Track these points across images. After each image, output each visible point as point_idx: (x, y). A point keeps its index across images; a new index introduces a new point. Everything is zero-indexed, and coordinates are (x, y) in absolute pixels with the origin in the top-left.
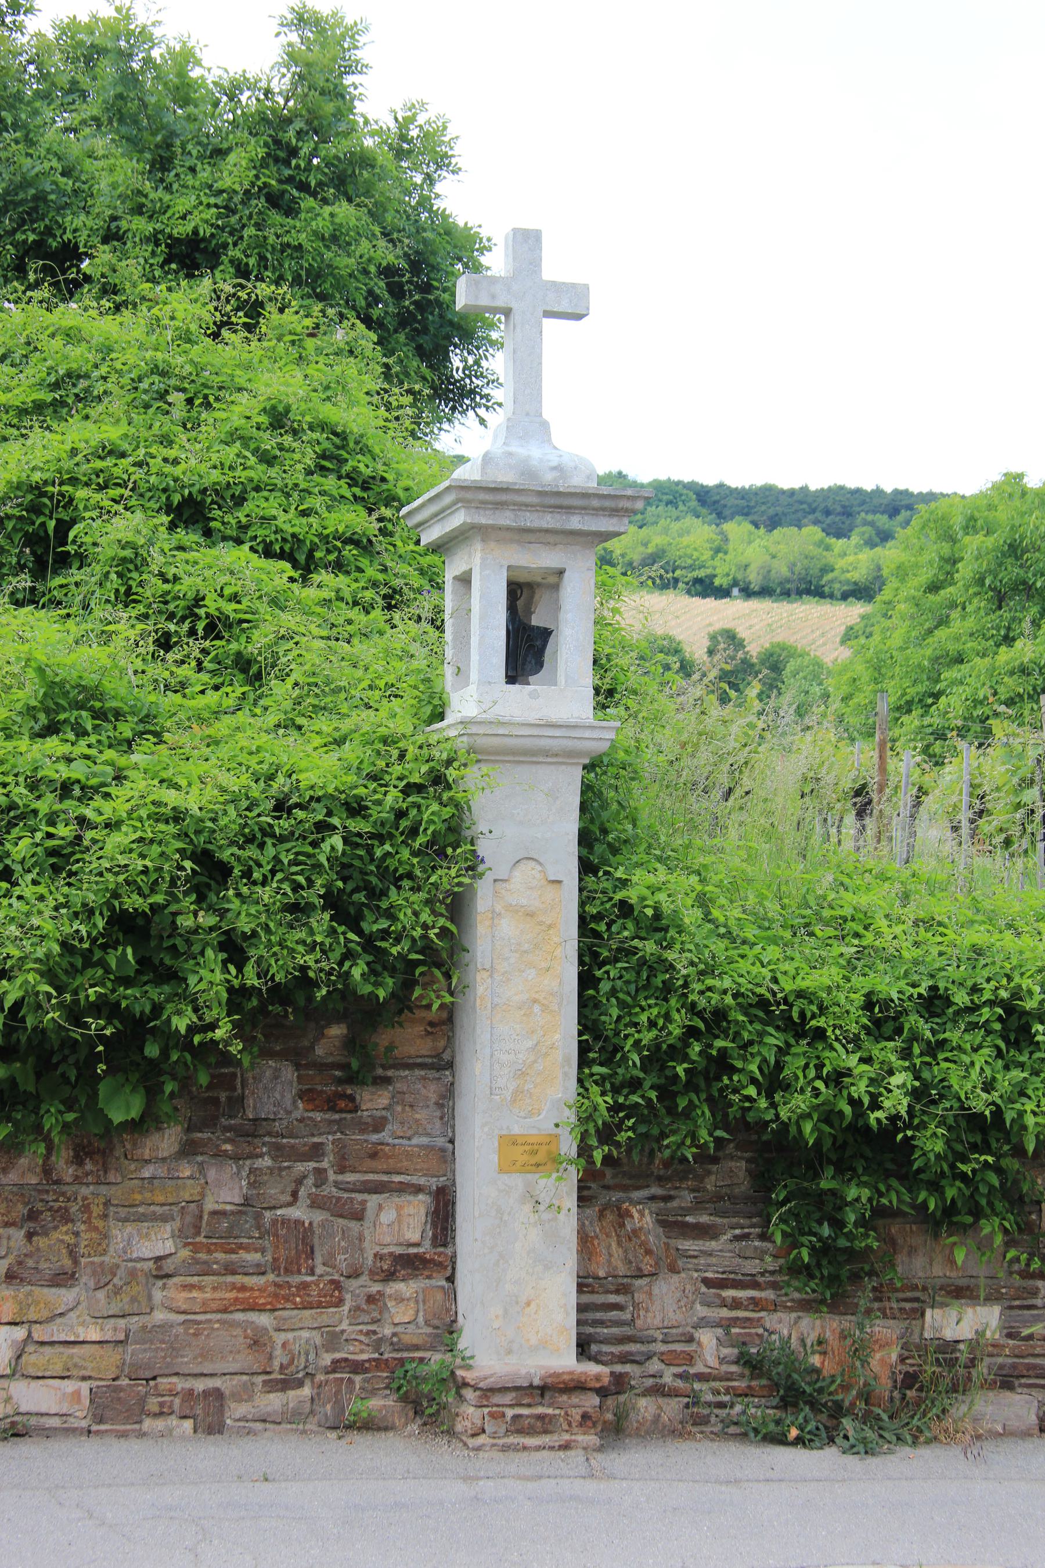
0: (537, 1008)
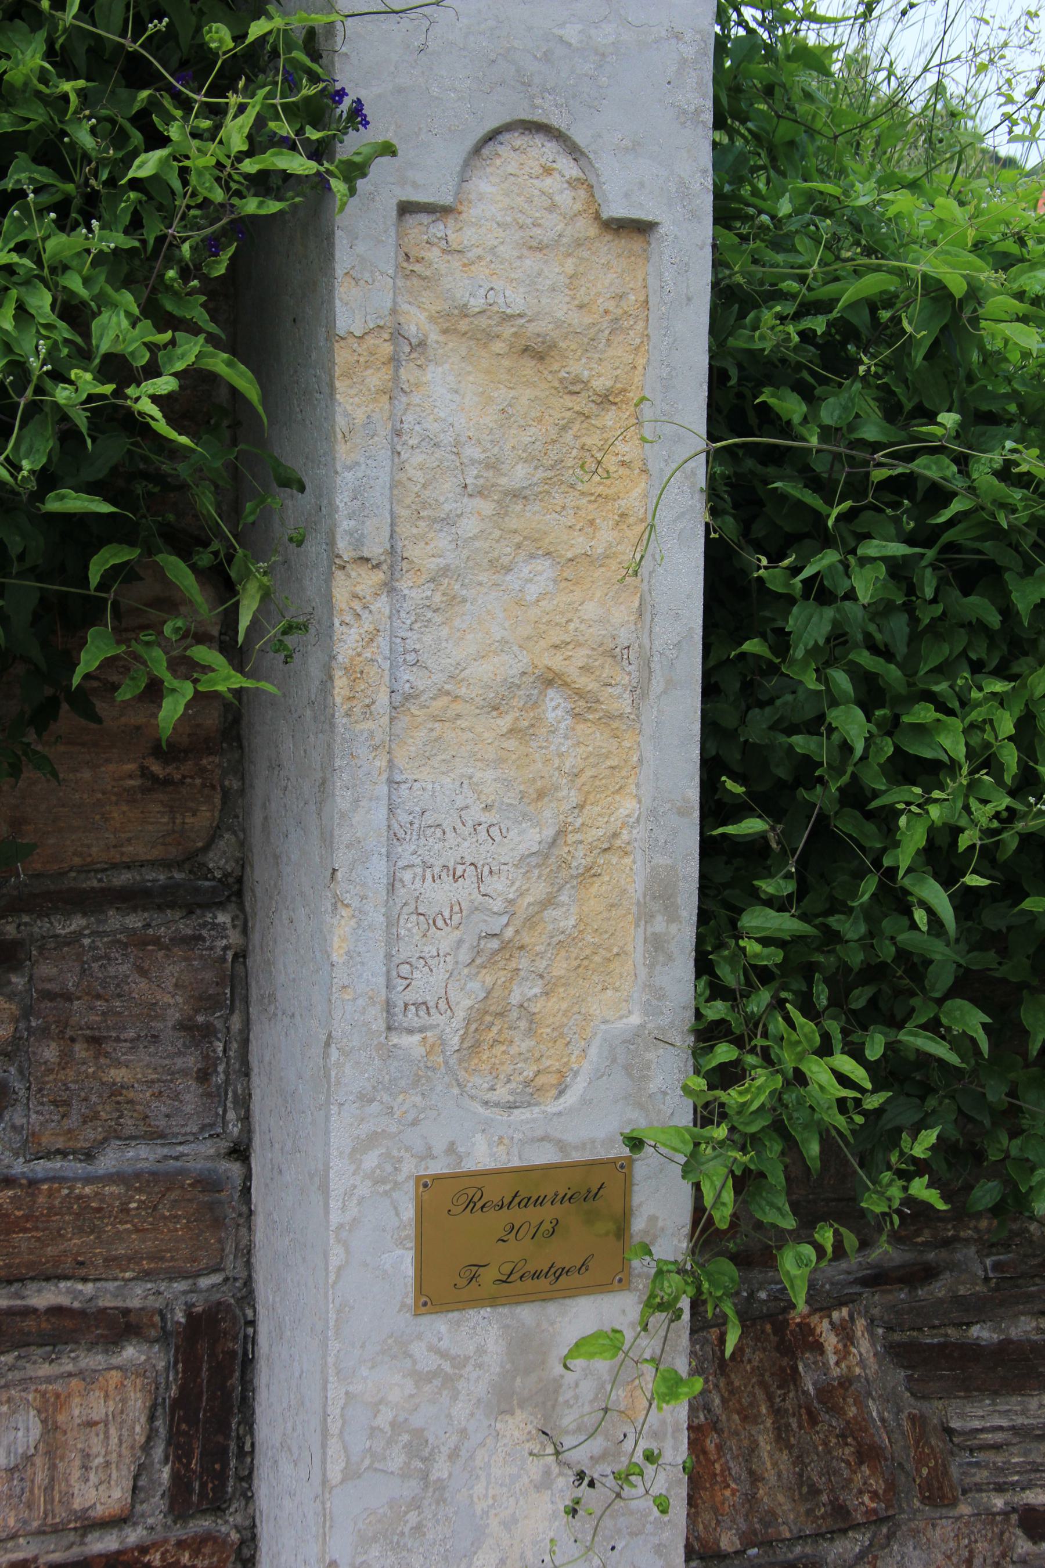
0: (555, 706)
